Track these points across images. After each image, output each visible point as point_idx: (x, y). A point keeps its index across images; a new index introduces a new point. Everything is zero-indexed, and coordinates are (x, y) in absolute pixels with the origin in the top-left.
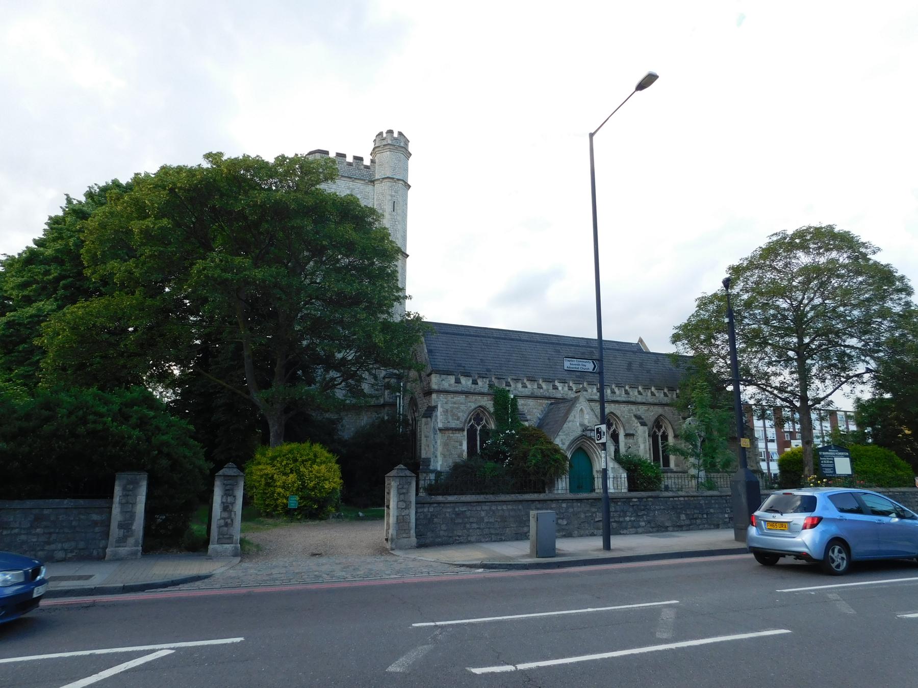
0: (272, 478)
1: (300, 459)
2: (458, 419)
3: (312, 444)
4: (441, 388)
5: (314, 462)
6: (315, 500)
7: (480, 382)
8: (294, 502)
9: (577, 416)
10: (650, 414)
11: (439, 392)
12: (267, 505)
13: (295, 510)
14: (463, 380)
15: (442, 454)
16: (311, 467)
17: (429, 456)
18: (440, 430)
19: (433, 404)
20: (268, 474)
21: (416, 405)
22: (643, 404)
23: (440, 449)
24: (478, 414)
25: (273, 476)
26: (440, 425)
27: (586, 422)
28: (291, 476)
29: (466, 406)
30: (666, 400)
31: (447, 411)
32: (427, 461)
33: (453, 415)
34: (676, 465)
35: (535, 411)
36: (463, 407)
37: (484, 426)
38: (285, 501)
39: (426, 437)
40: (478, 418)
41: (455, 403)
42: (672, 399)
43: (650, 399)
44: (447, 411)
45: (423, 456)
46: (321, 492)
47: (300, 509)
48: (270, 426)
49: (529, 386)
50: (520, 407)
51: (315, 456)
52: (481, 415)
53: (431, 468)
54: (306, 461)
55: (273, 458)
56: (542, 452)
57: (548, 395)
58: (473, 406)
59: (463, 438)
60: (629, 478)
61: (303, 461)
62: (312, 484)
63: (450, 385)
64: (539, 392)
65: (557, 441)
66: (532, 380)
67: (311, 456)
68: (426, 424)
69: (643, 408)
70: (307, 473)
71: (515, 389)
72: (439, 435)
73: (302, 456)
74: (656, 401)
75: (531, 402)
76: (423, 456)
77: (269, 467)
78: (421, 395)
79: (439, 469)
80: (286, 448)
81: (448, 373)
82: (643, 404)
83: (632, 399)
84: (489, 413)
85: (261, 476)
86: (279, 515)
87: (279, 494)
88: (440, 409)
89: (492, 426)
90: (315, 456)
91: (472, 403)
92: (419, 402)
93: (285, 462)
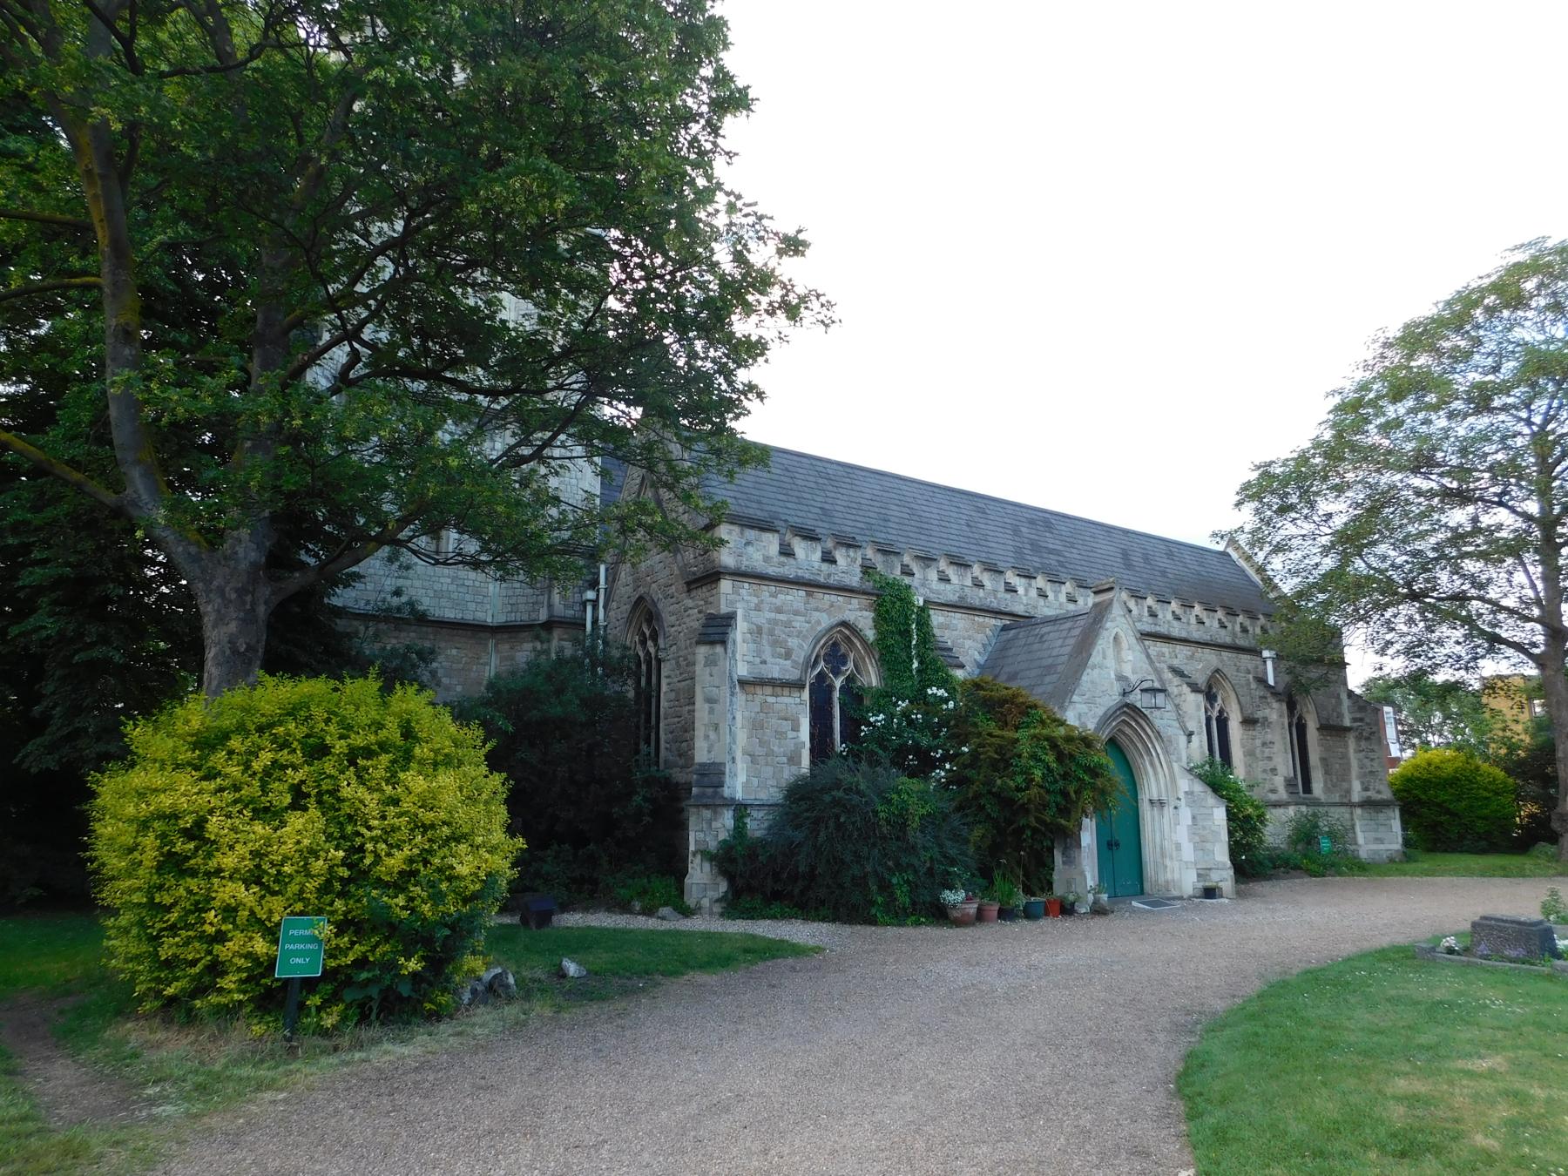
0: (196, 832)
1: (340, 747)
2: (788, 656)
3: (387, 689)
4: (745, 564)
5: (405, 759)
6: (413, 937)
7: (839, 555)
8: (303, 950)
9: (1110, 652)
10: (1201, 664)
11: (739, 574)
12: (168, 964)
13: (309, 985)
14: (799, 547)
15: (745, 753)
16: (392, 780)
17: (716, 756)
18: (743, 683)
19: (724, 609)
20: (175, 816)
21: (805, 538)
22: (1184, 641)
23: (742, 737)
24: (835, 645)
25: (201, 823)
26: (742, 670)
27: (1127, 671)
28: (296, 821)
29: (808, 621)
30: (1224, 637)
31: (759, 630)
32: (713, 775)
33: (775, 643)
34: (1327, 790)
35: (968, 643)
36: (799, 622)
37: (850, 679)
38: (260, 946)
39: (710, 700)
40: (834, 655)
41: (779, 610)
42: (1234, 634)
43: (1196, 633)
44: (759, 630)
45: (701, 755)
46: (437, 897)
47: (335, 981)
48: (208, 621)
49: (954, 579)
50: (936, 631)
51: (408, 733)
52: (843, 648)
53: (726, 792)
54: (368, 753)
55: (208, 742)
56: (1054, 745)
57: (995, 605)
58: (826, 621)
59: (799, 705)
60: (1231, 817)
61: (352, 757)
62: (396, 862)
63: (767, 559)
64: (977, 597)
65: (1071, 717)
66: (961, 564)
67: (392, 732)
68: (711, 662)
69: (1183, 651)
70: (372, 801)
71: (925, 585)
72: (740, 697)
73: (347, 729)
74: (1206, 638)
75: (959, 620)
76: (701, 755)
77: (185, 781)
78: (678, 587)
79: (739, 795)
80: (274, 693)
81: (765, 526)
82: (1184, 641)
83: (1163, 630)
84: (863, 640)
85: (144, 826)
86: (229, 1012)
87: (229, 912)
88: (741, 628)
89: (872, 677)
90: (408, 733)
91: (826, 612)
92: (667, 611)
93: (266, 757)
